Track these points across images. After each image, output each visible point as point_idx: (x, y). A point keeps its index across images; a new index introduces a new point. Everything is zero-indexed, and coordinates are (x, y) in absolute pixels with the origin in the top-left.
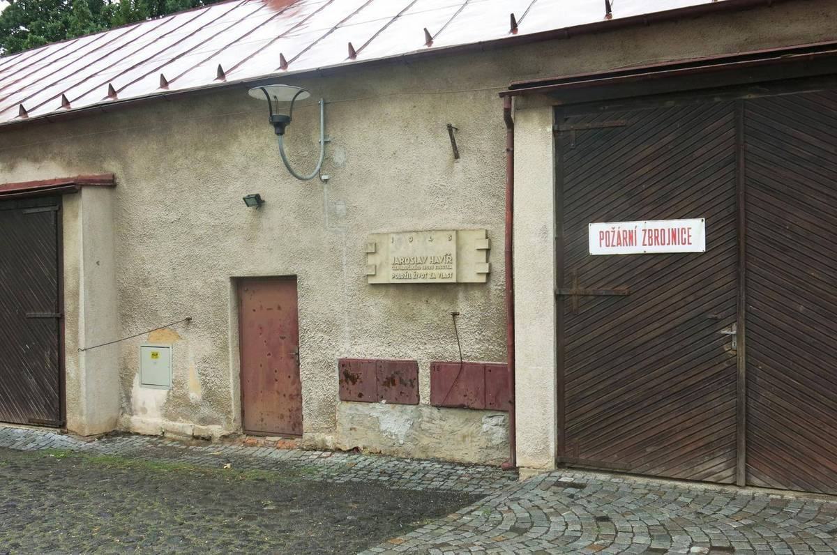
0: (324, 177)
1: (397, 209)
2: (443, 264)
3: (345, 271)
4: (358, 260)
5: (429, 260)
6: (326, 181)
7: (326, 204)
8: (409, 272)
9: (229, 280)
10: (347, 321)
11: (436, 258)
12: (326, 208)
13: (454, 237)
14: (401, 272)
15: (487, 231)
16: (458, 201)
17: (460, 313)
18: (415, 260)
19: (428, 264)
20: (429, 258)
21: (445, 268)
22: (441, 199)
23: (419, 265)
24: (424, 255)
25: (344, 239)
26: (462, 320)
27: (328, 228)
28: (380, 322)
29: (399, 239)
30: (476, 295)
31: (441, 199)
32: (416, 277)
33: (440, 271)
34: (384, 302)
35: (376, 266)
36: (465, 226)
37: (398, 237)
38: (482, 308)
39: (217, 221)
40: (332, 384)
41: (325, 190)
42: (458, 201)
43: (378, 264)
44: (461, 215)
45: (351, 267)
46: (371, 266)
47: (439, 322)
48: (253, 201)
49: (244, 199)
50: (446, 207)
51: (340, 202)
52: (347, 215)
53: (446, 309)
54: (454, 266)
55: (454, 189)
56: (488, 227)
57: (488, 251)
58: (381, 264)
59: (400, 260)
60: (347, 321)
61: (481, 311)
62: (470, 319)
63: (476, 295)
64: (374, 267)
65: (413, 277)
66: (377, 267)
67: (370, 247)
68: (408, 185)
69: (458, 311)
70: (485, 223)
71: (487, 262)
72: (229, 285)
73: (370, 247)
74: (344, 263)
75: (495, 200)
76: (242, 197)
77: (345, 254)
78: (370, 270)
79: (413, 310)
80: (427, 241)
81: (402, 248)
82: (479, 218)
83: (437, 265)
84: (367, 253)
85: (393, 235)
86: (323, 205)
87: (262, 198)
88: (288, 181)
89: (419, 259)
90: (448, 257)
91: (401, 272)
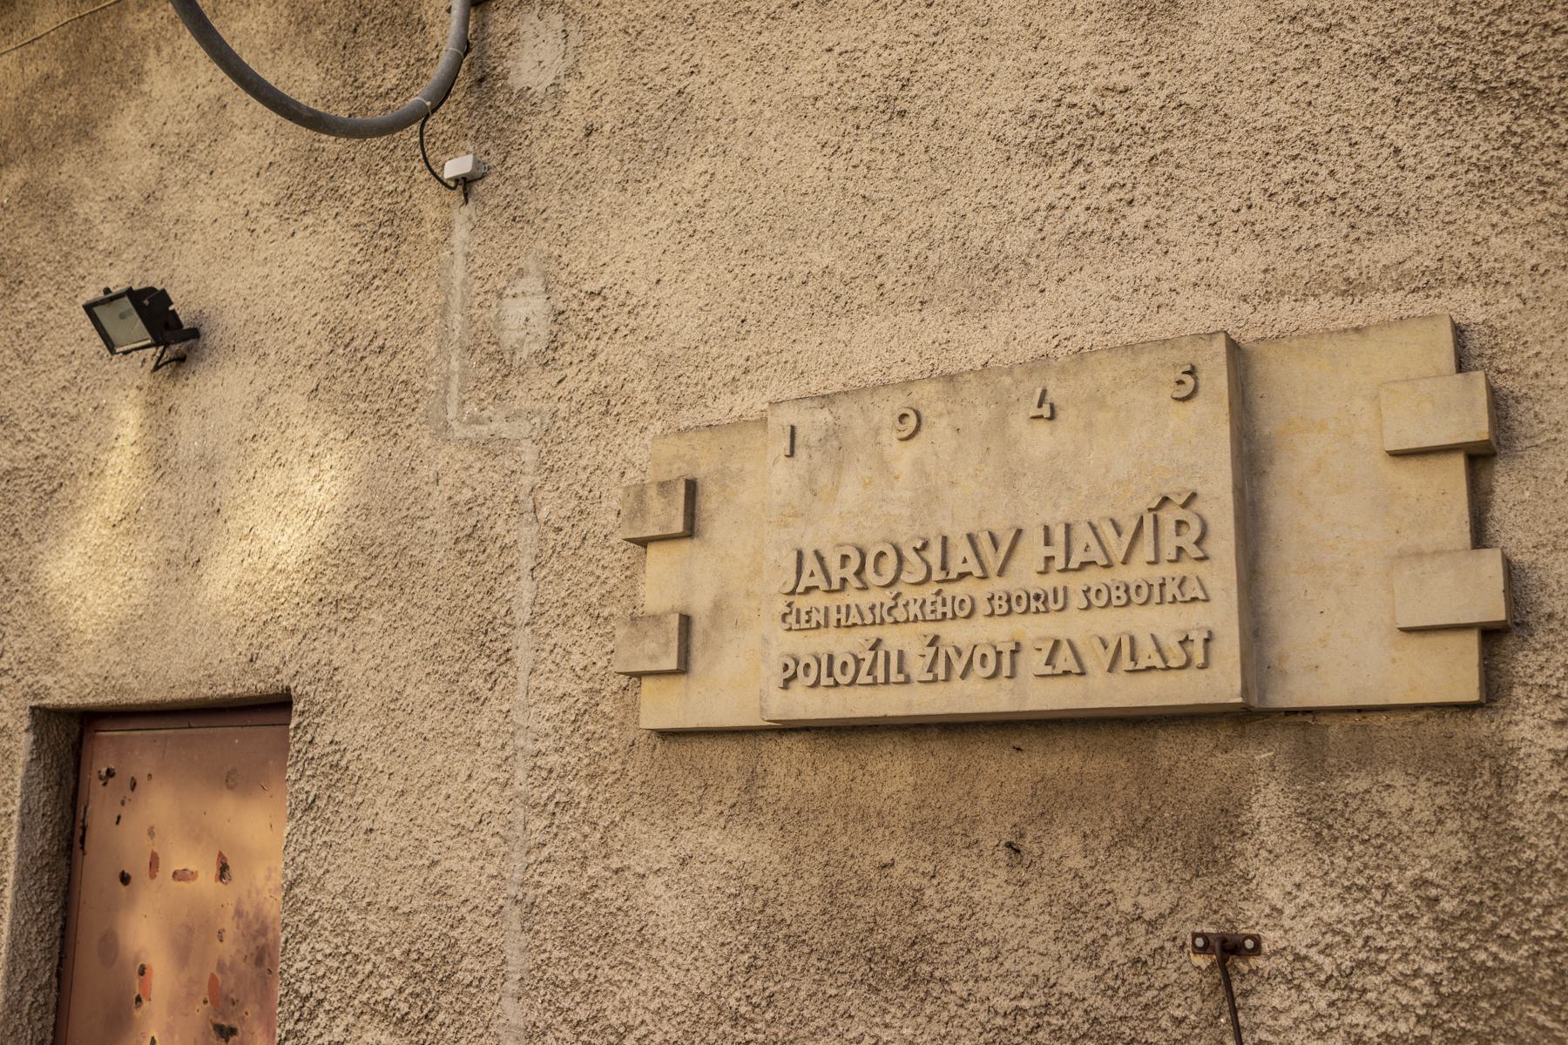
0: (455, 167)
1: (827, 271)
2: (1137, 572)
3: (523, 658)
4: (594, 596)
5: (1032, 552)
6: (465, 184)
7: (456, 301)
8: (894, 638)
9: (27, 723)
10: (517, 963)
11: (1083, 536)
12: (456, 319)
13: (1216, 379)
14: (844, 644)
15: (1459, 332)
16: (1225, 164)
17: (1271, 939)
18: (934, 556)
19: (1025, 575)
20: (1034, 537)
21: (1156, 594)
22: (1106, 175)
23: (959, 590)
24: (1001, 524)
25: (526, 481)
26: (1278, 997)
27: (459, 431)
28: (701, 978)
29: (834, 433)
30: (1397, 801)
31: (1106, 175)
32: (943, 665)
33: (1112, 623)
34: (732, 849)
35: (686, 621)
36: (1285, 313)
37: (823, 416)
38: (1448, 905)
39: (20, 452)
40: (1050, 667)
41: (460, 234)
42: (1225, 164)
43: (700, 607)
44: (1251, 249)
45: (559, 636)
46: (657, 619)
47: (1095, 1000)
48: (132, 329)
49: (89, 308)
50: (1138, 216)
51: (523, 284)
52: (554, 343)
53: (1152, 906)
54: (1222, 575)
55: (1191, 98)
56: (1470, 305)
57: (1479, 458)
58: (717, 607)
59: (833, 563)
60: (517, 963)
61: (1441, 925)
62: (1345, 985)
63: (1397, 801)
64: (674, 621)
65: (917, 668)
66: (698, 628)
67: (655, 503)
68: (896, 127)
69: (1250, 919)
70: (1429, 282)
71: (1480, 537)
72: (23, 743)
73: (655, 503)
74: (522, 616)
75: (1498, 120)
76: (81, 301)
77: (526, 563)
78: (651, 646)
79: (917, 904)
80: (1019, 423)
81: (851, 492)
82: (1387, 250)
83: (1093, 578)
84: (644, 543)
85: (788, 416)
86: (444, 311)
87: (184, 306)
88: (308, 220)
89: (964, 550)
90: (1168, 517)
91: (844, 644)
